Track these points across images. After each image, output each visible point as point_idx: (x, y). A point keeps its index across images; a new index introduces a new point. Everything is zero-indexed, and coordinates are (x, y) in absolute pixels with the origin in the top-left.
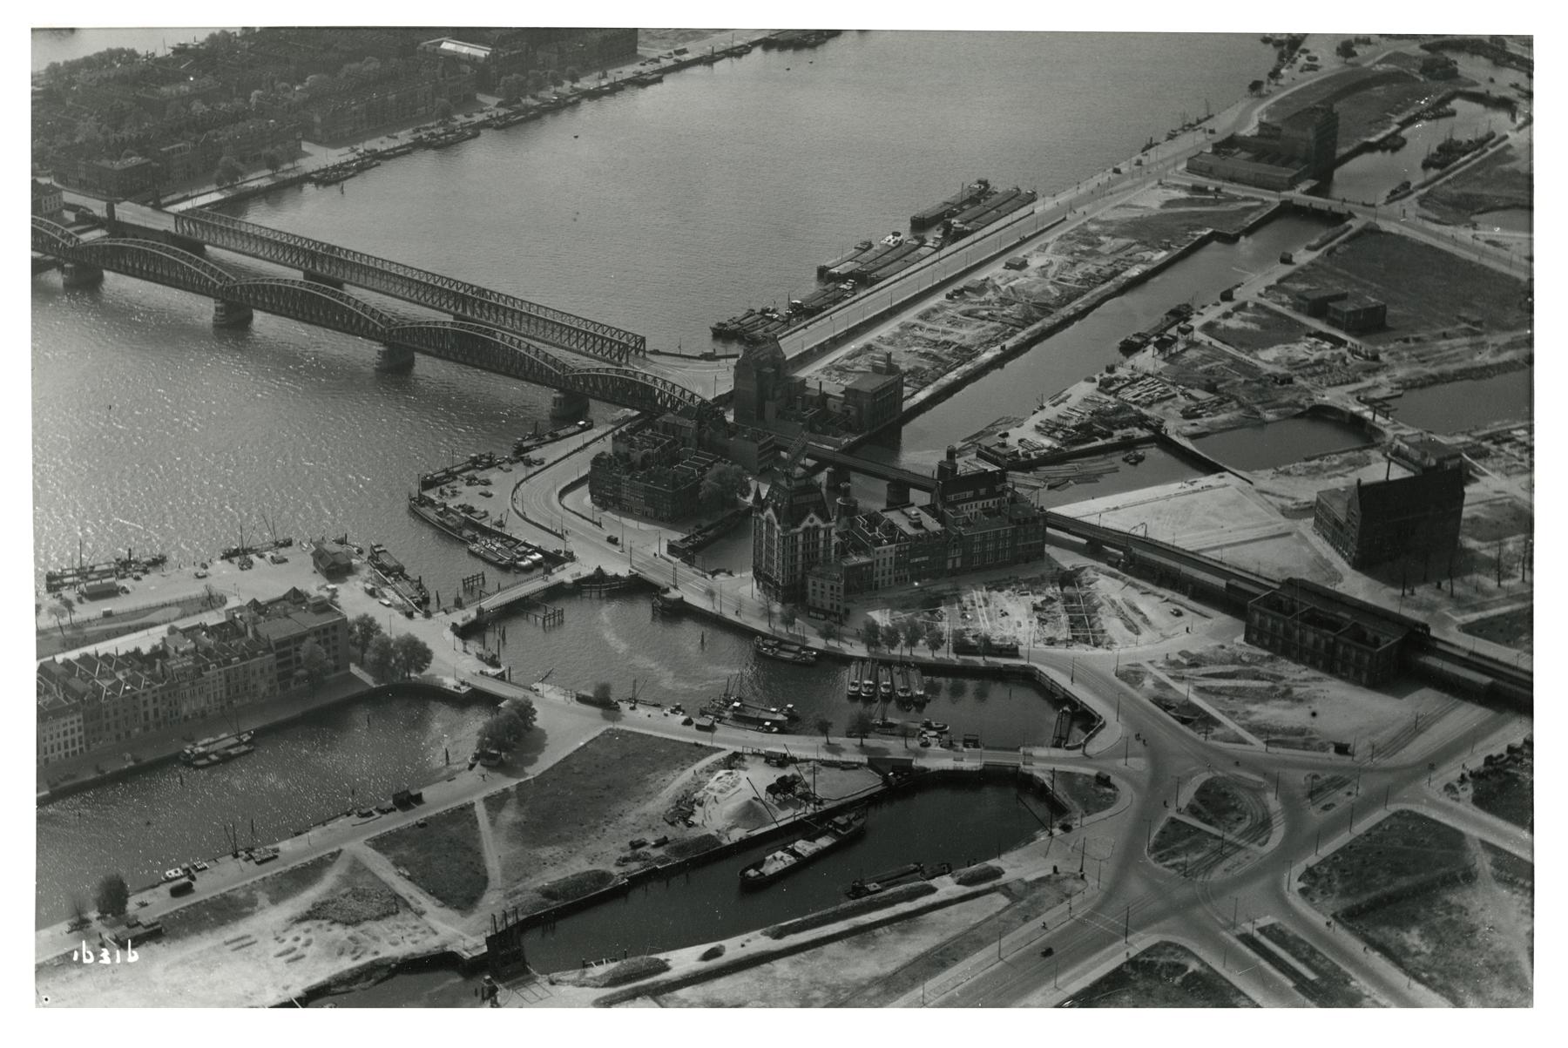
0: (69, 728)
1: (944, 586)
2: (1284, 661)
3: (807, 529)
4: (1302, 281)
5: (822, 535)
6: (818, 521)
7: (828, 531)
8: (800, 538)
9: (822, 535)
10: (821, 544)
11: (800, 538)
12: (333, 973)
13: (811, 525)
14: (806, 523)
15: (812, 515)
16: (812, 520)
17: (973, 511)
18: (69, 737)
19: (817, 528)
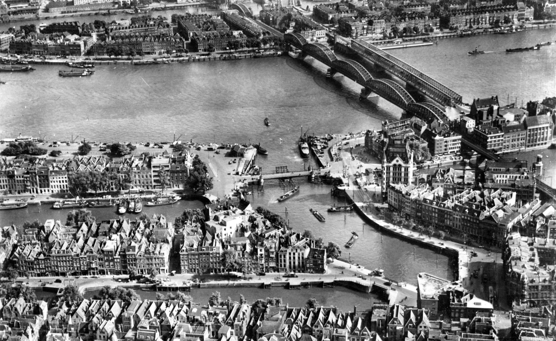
0: (61, 180)
1: (486, 221)
2: (355, 214)
3: (395, 165)
4: (5, 277)
5: (403, 169)
6: (401, 162)
7: (407, 169)
8: (391, 169)
9: (403, 169)
10: (403, 175)
11: (391, 169)
12: (522, 54)
13: (397, 164)
14: (394, 162)
15: (397, 159)
16: (397, 161)
17: (505, 179)
18: (62, 184)
19: (400, 165)
